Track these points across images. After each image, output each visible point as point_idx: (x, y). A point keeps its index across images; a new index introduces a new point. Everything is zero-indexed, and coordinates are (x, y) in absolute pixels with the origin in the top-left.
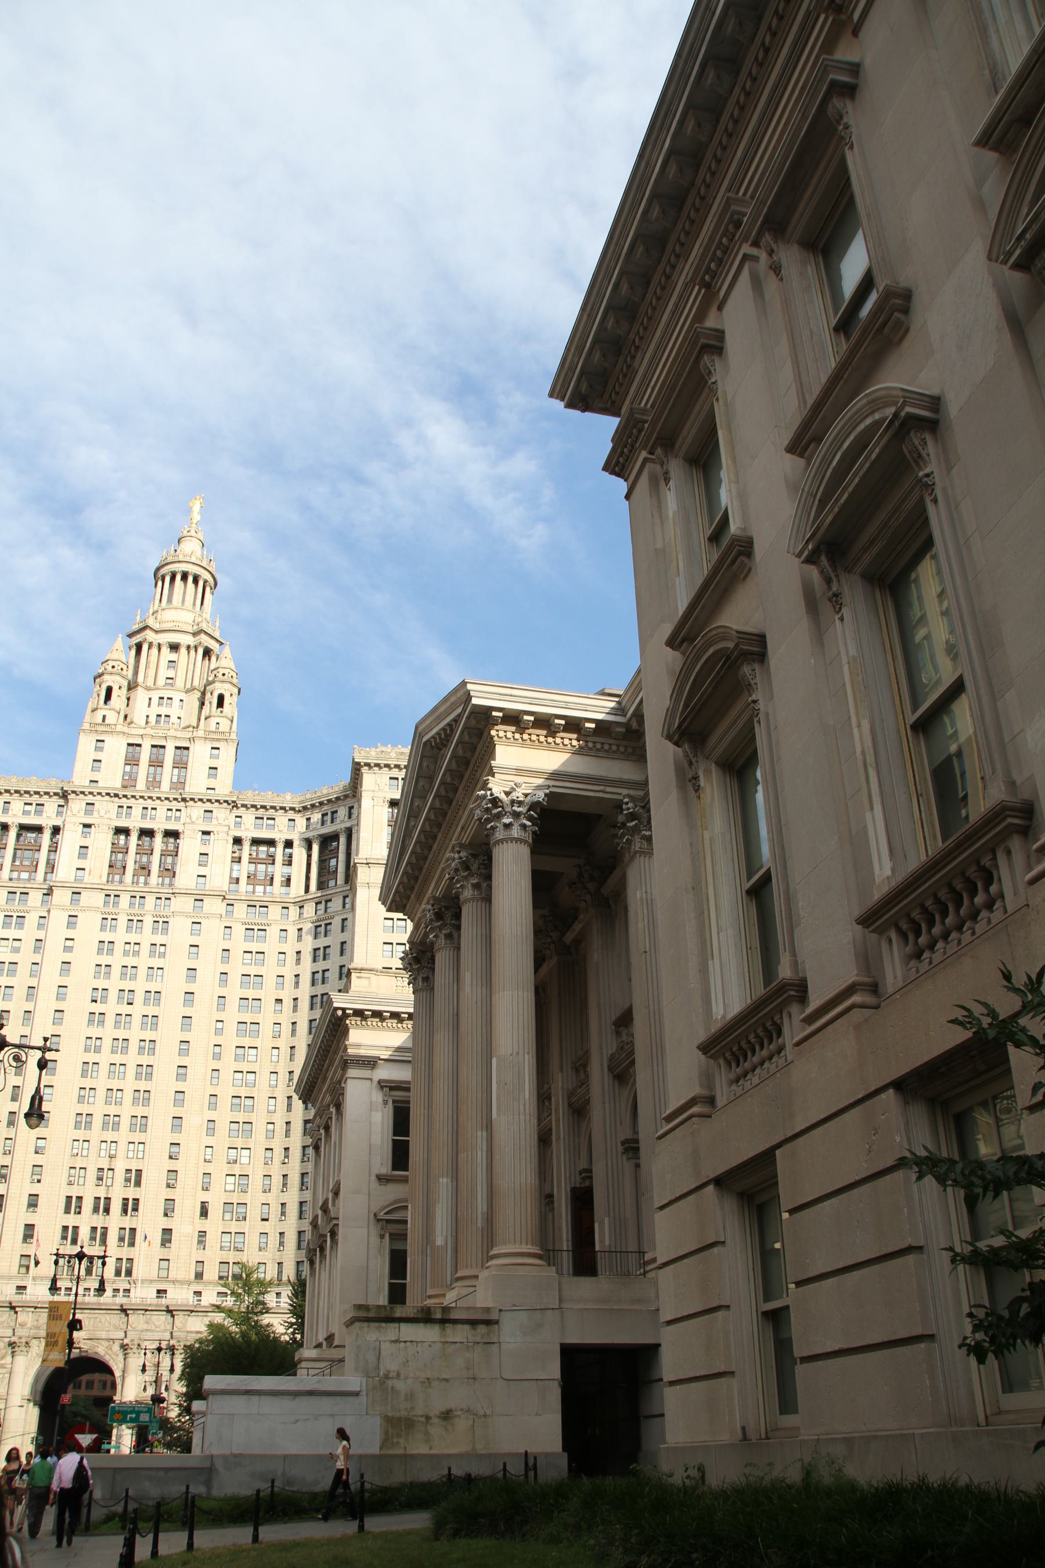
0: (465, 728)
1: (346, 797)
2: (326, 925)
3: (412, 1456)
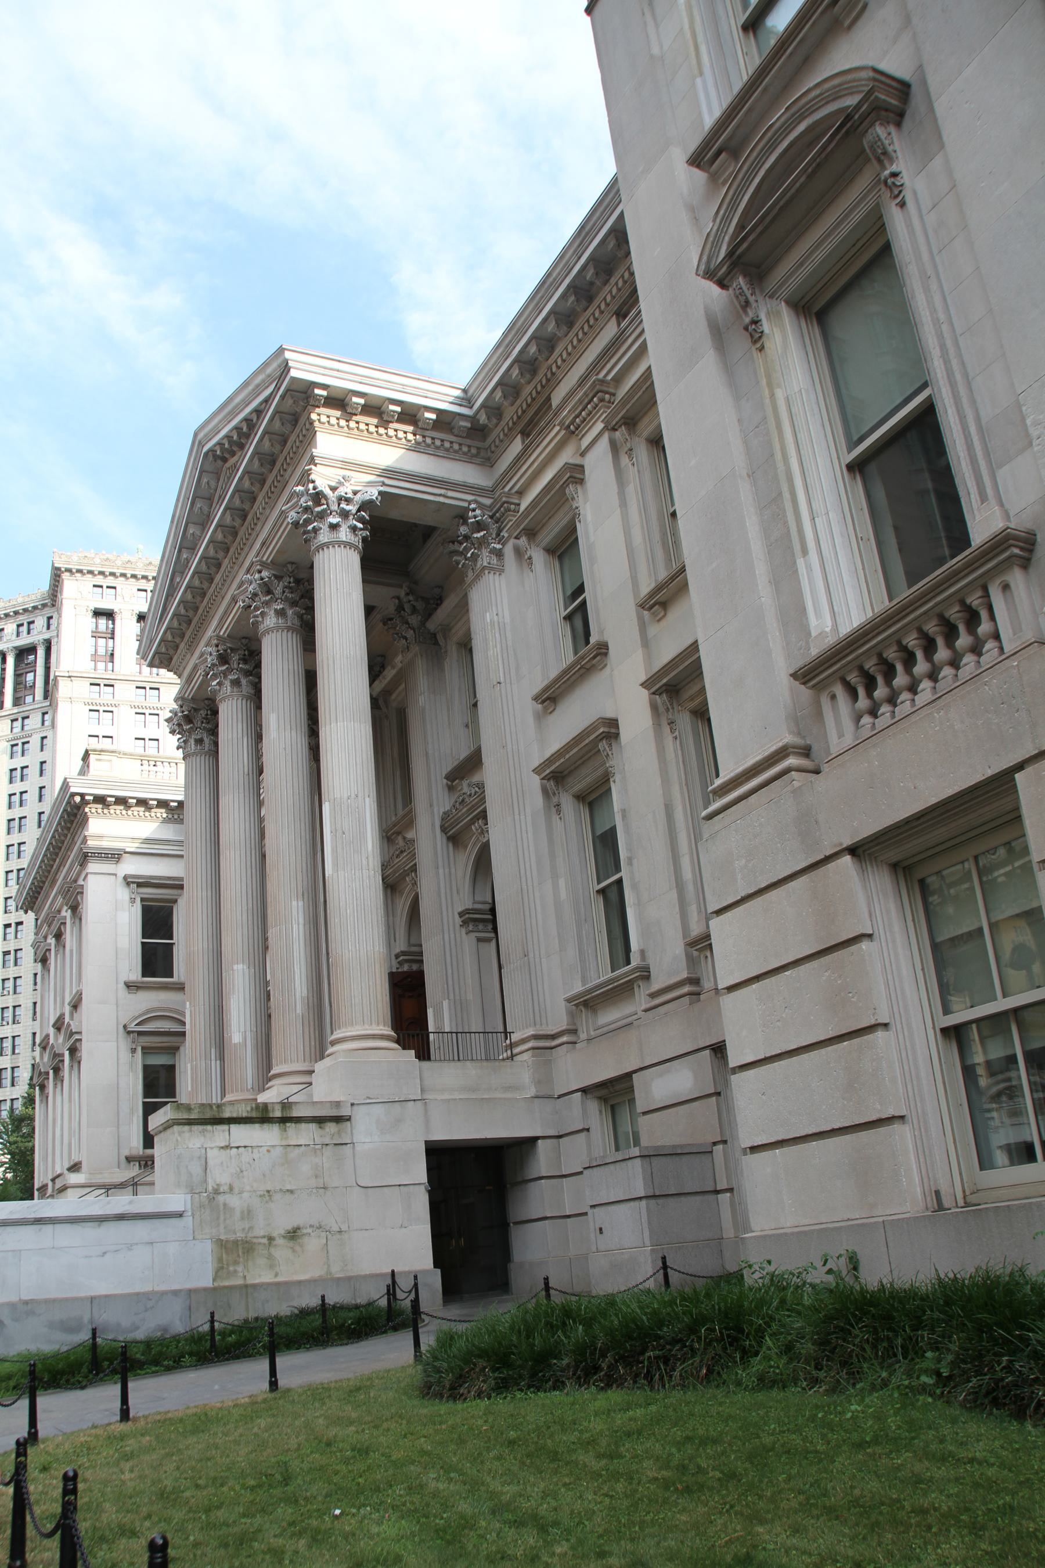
0: (276, 412)
1: (44, 606)
2: (24, 744)
3: (254, 1286)
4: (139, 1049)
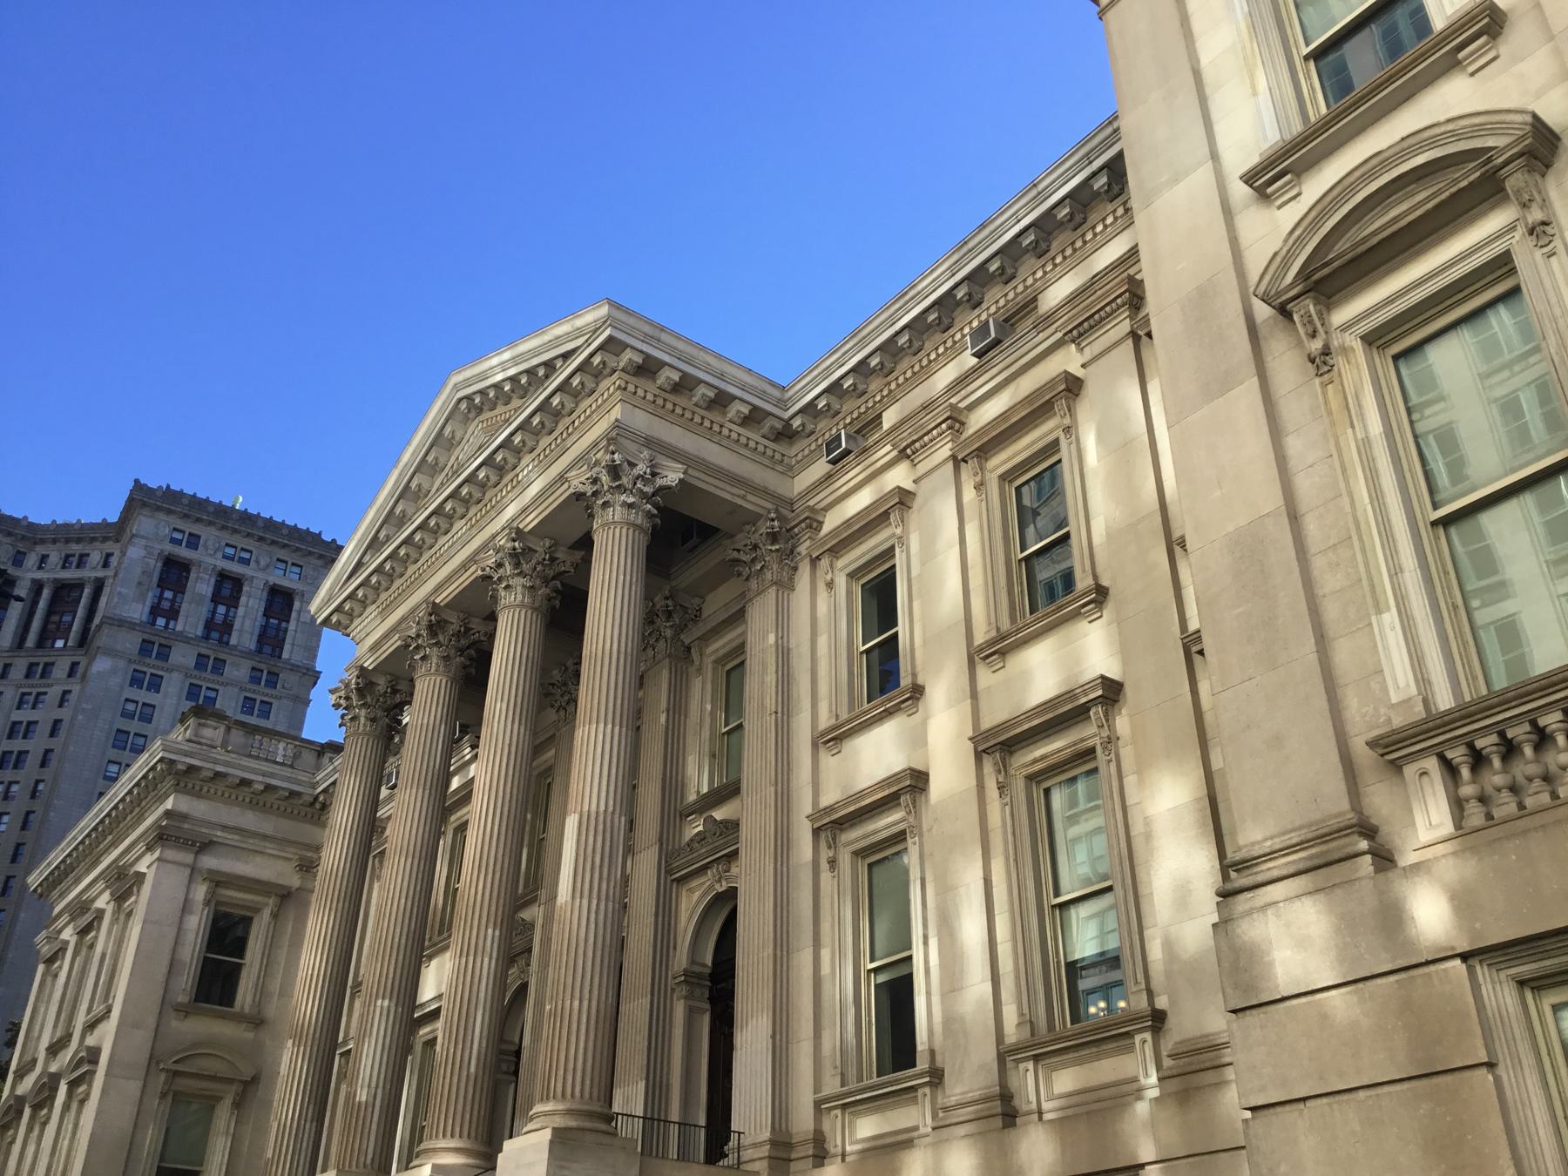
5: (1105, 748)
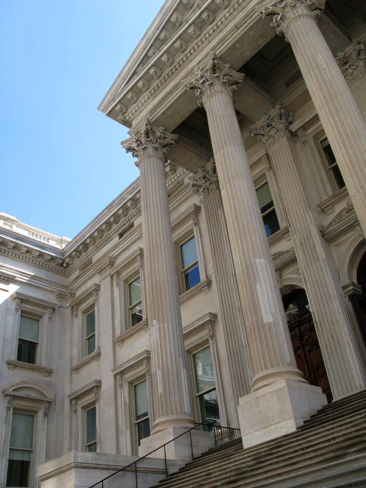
4: (12, 409)
5: (212, 338)
